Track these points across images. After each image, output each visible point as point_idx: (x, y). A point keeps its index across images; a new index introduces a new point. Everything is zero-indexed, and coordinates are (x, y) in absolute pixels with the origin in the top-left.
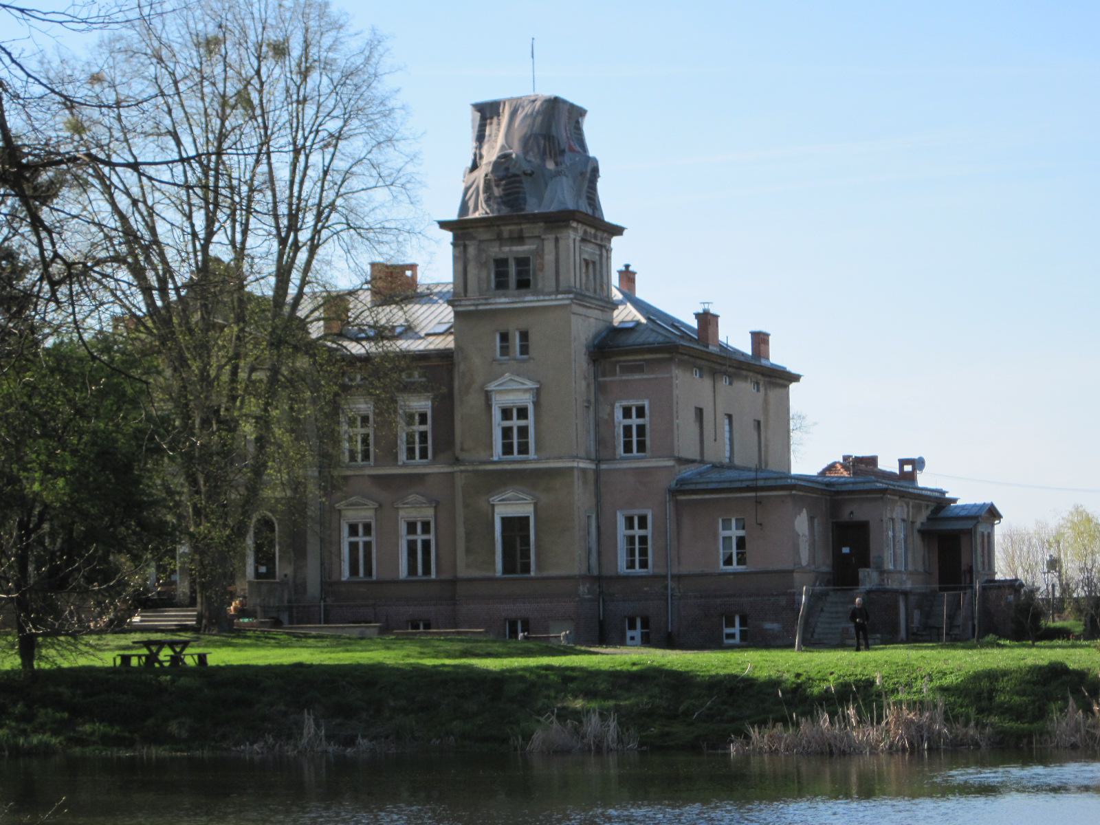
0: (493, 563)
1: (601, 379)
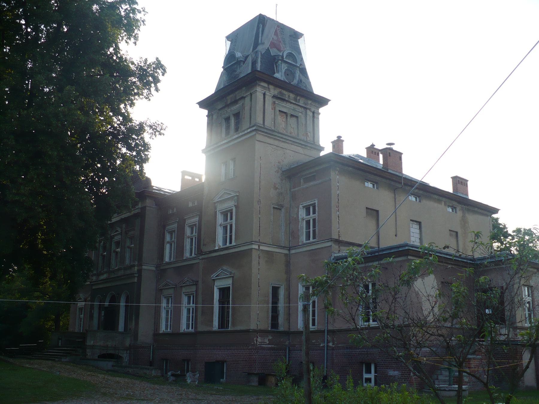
0: (212, 321)
1: (293, 190)
